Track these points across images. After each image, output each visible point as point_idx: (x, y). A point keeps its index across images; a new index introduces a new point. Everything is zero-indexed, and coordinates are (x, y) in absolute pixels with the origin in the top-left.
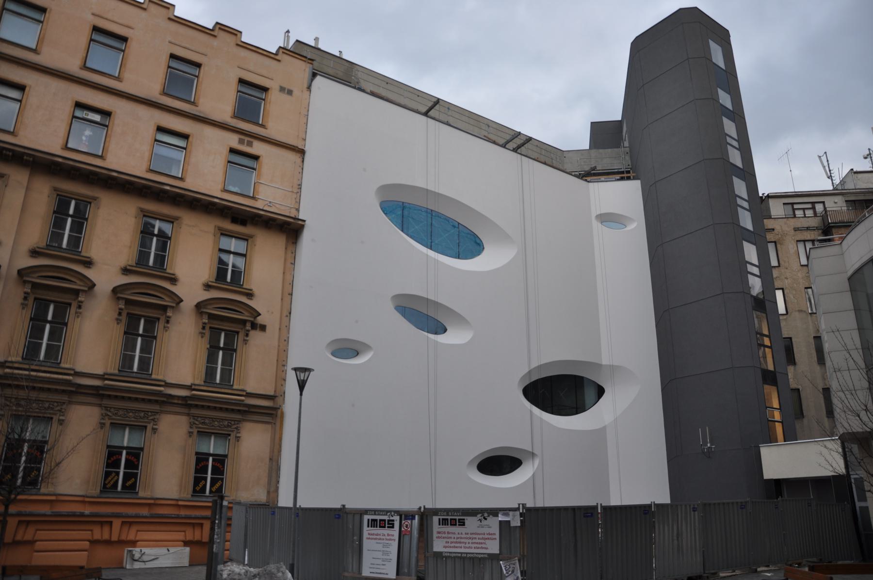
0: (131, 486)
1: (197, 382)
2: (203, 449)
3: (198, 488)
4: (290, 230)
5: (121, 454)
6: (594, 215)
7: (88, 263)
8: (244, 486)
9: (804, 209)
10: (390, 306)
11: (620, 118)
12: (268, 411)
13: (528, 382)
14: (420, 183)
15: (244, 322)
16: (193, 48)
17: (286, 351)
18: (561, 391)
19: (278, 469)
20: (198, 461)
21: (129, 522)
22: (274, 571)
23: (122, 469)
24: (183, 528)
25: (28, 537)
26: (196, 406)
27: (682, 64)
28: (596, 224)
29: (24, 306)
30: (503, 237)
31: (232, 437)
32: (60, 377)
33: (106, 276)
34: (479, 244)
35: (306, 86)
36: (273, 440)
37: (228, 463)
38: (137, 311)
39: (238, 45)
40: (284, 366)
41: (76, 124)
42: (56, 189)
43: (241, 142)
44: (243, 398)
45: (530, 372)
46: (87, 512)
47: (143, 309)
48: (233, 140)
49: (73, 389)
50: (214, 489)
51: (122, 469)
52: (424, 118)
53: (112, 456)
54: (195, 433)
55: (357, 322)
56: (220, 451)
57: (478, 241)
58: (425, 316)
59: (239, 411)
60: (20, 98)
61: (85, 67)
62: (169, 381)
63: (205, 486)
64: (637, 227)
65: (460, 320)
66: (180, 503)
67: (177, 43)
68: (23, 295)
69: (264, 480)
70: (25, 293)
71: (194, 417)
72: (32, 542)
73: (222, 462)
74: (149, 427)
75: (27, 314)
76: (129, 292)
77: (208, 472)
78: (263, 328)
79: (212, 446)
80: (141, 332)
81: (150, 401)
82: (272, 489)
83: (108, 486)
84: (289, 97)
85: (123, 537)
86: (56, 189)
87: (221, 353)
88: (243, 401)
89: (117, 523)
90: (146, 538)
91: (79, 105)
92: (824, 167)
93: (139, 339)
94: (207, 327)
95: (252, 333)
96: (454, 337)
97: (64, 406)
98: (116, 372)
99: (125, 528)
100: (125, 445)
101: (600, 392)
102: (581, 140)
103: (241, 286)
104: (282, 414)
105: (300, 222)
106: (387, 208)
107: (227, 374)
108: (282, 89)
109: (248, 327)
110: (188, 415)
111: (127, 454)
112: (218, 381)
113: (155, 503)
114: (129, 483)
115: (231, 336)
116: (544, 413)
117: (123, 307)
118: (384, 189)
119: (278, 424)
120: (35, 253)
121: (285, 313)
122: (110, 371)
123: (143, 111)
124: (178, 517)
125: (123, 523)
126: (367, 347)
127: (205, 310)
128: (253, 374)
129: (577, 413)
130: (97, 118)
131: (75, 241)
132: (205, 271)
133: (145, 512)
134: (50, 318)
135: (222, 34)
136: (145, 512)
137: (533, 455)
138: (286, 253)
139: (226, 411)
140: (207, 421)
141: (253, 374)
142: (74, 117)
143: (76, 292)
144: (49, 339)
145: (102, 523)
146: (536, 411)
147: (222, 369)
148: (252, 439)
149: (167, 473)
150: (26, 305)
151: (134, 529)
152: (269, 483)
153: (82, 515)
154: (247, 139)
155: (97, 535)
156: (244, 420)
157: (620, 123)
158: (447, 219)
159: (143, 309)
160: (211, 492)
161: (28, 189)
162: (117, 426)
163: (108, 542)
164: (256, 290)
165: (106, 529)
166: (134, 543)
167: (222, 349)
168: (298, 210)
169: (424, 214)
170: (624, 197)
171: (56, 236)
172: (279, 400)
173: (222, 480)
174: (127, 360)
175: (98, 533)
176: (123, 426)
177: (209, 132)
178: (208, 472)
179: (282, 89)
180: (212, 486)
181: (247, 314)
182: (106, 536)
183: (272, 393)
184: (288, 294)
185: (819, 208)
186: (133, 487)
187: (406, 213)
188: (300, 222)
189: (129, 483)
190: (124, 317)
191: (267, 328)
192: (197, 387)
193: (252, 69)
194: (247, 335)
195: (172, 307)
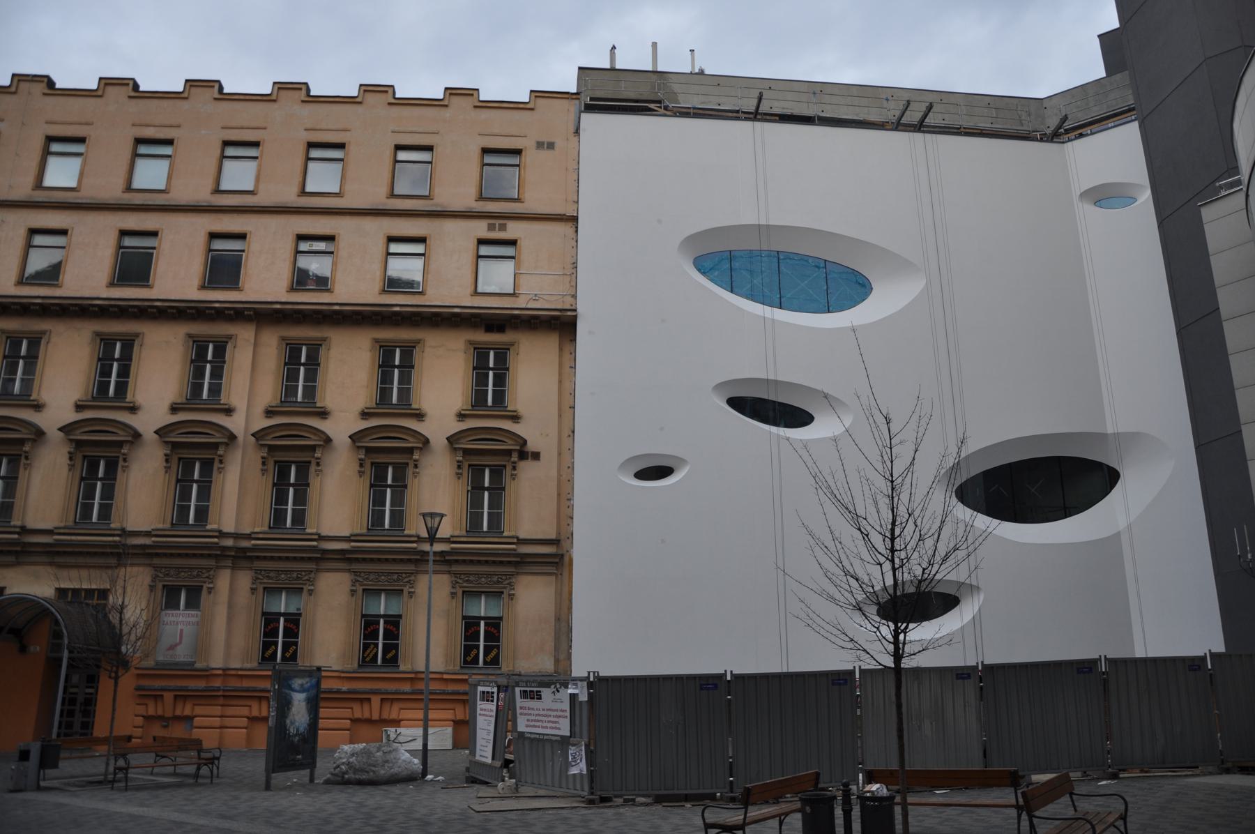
0: (392, 658)
1: (457, 533)
2: (473, 612)
3: (267, 655)
4: (562, 325)
5: (378, 623)
7: (323, 414)
8: (526, 651)
12: (553, 559)
16: (420, 130)
17: (571, 481)
18: (1040, 484)
19: (570, 630)
20: (367, 624)
21: (389, 699)
22: (374, 750)
23: (380, 639)
24: (451, 706)
25: (187, 712)
26: (457, 561)
29: (459, 476)
30: (898, 265)
31: (505, 596)
32: (73, 538)
33: (342, 424)
34: (863, 286)
35: (572, 129)
36: (559, 594)
37: (503, 625)
38: (381, 459)
39: (476, 107)
41: (482, 263)
42: (283, 339)
43: (491, 228)
46: (344, 689)
47: (388, 457)
48: (481, 229)
50: (488, 659)
51: (380, 639)
53: (369, 625)
54: (261, 590)
55: (662, 429)
56: (393, 611)
59: (509, 562)
60: (422, 251)
61: (392, 195)
63: (275, 652)
66: (445, 676)
67: (401, 129)
68: (260, 461)
69: (550, 645)
71: (456, 574)
72: (190, 719)
73: (297, 623)
74: (406, 590)
75: (269, 479)
77: (481, 641)
78: (536, 456)
79: (482, 608)
80: (389, 482)
81: (402, 560)
82: (562, 657)
83: (367, 660)
84: (550, 152)
85: (385, 716)
86: (471, 343)
87: (486, 494)
89: (376, 700)
90: (410, 716)
91: (301, 238)
93: (389, 491)
94: (466, 465)
95: (523, 465)
97: (312, 575)
98: (364, 531)
99: (387, 706)
100: (282, 611)
104: (571, 560)
105: (569, 313)
106: (704, 265)
107: (495, 520)
108: (540, 145)
109: (515, 458)
110: (449, 572)
111: (385, 622)
112: (485, 529)
113: (415, 677)
114: (389, 656)
115: (497, 472)
118: (692, 240)
119: (566, 573)
120: (269, 413)
121: (566, 432)
122: (358, 531)
123: (369, 224)
124: (444, 693)
125: (176, 697)
126: (682, 461)
128: (527, 516)
130: (321, 246)
131: (310, 392)
132: (268, 392)
133: (407, 687)
135: (455, 100)
136: (407, 687)
137: (973, 589)
138: (560, 356)
139: (505, 564)
140: (472, 578)
141: (527, 516)
142: (479, 257)
143: (410, 451)
144: (198, 500)
145: (362, 701)
147: (489, 514)
148: (531, 597)
149: (431, 639)
151: (396, 707)
152: (557, 648)
153: (339, 692)
154: (497, 222)
155: (358, 715)
156: (518, 573)
158: (804, 259)
159: (388, 457)
160: (485, 662)
161: (256, 345)
162: (272, 591)
163: (370, 721)
165: (366, 707)
166: (396, 723)
168: (574, 296)
171: (290, 391)
172: (565, 544)
173: (498, 647)
174: (377, 518)
175: (358, 711)
176: (378, 592)
177: (450, 225)
178: (481, 641)
179: (540, 145)
180: (486, 655)
181: (510, 442)
182: (367, 715)
183: (553, 536)
184: (566, 406)
186: (394, 660)
188: (569, 313)
189: (389, 656)
190: (465, 471)
193: (496, 131)
194: (514, 468)
195: (421, 449)
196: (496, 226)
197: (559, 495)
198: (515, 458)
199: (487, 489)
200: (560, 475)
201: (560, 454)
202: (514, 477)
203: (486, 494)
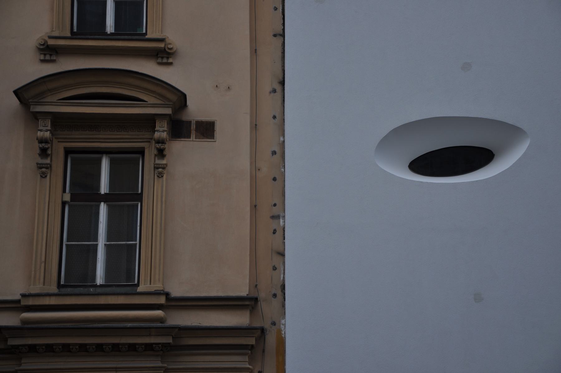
15: (148, 122)
26: (33, 349)
29: (43, 170)
40: (276, 217)
44: (159, 313)
49: (169, 340)
59: (149, 347)
62: (177, 292)
70: (41, 141)
76: (54, 98)
78: (207, 130)
87: (103, 209)
88: (161, 320)
94: (59, 149)
95: (178, 148)
103: (142, 37)
109: (162, 131)
115: (127, 164)
117: (47, 134)
121: (267, 83)
126: (512, 133)
127: (39, 109)
134: (104, 188)
147: (108, 247)
150: (49, 167)
164: (174, 38)
167: (106, 198)
172: (267, 309)
174: (79, 259)
181: (151, 100)
191: (217, 128)
192: (31, 302)
194: (161, 153)
196: (43, 173)
197: (254, 207)
198: (162, 131)
199: (106, 198)
200: (255, 168)
201: (255, 127)
202: (160, 171)
203: (103, 209)
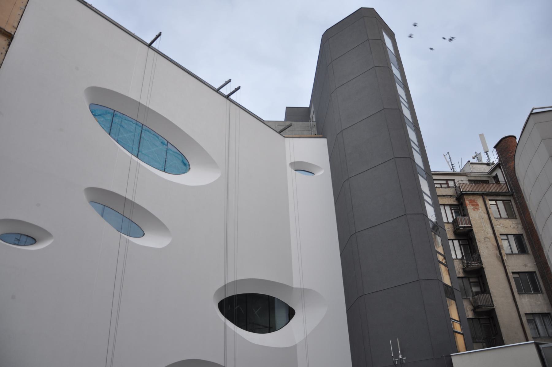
6: (288, 162)
9: (441, 184)
10: (84, 198)
11: (308, 106)
13: (223, 298)
14: (134, 95)
27: (357, 51)
28: (290, 171)
30: (208, 161)
34: (185, 164)
45: (226, 286)
52: (147, 48)
57: (185, 161)
58: (123, 214)
64: (324, 173)
65: (159, 226)
92: (448, 162)
96: (151, 241)
101: (291, 313)
102: (281, 117)
106: (97, 110)
116: (238, 328)
126: (47, 235)
129: (270, 332)
146: (231, 325)
157: (308, 110)
169: (134, 125)
170: (313, 150)
185: (451, 184)
187: (116, 120)
